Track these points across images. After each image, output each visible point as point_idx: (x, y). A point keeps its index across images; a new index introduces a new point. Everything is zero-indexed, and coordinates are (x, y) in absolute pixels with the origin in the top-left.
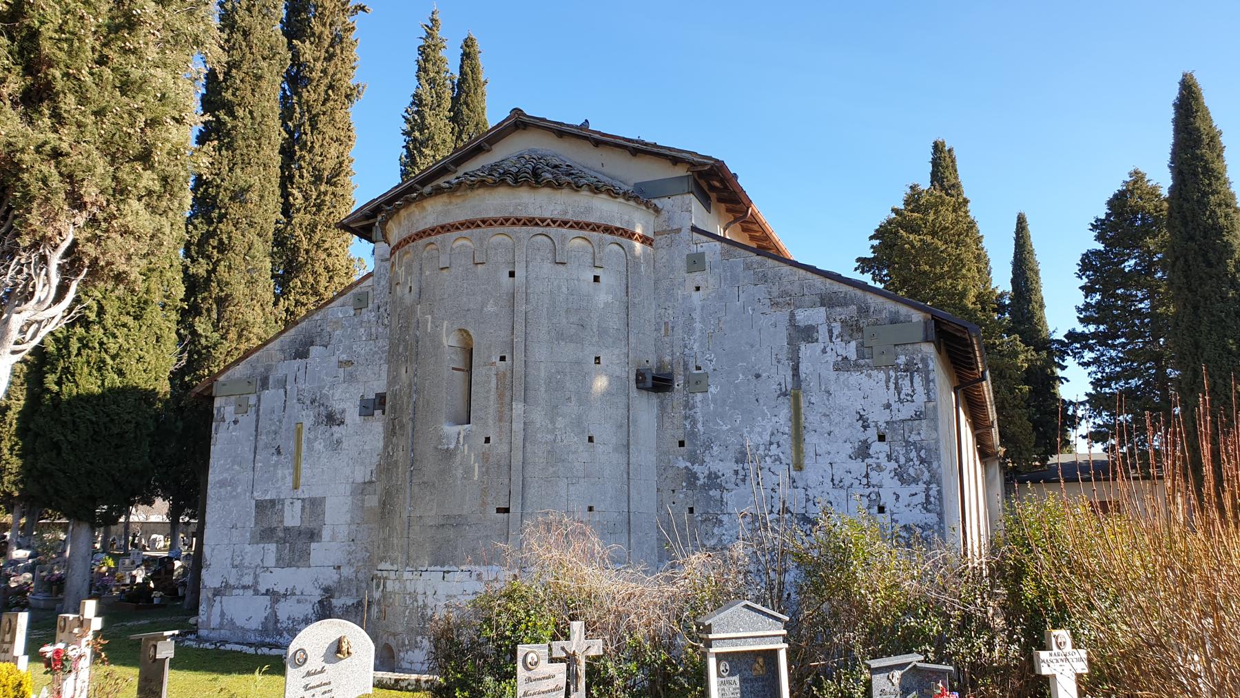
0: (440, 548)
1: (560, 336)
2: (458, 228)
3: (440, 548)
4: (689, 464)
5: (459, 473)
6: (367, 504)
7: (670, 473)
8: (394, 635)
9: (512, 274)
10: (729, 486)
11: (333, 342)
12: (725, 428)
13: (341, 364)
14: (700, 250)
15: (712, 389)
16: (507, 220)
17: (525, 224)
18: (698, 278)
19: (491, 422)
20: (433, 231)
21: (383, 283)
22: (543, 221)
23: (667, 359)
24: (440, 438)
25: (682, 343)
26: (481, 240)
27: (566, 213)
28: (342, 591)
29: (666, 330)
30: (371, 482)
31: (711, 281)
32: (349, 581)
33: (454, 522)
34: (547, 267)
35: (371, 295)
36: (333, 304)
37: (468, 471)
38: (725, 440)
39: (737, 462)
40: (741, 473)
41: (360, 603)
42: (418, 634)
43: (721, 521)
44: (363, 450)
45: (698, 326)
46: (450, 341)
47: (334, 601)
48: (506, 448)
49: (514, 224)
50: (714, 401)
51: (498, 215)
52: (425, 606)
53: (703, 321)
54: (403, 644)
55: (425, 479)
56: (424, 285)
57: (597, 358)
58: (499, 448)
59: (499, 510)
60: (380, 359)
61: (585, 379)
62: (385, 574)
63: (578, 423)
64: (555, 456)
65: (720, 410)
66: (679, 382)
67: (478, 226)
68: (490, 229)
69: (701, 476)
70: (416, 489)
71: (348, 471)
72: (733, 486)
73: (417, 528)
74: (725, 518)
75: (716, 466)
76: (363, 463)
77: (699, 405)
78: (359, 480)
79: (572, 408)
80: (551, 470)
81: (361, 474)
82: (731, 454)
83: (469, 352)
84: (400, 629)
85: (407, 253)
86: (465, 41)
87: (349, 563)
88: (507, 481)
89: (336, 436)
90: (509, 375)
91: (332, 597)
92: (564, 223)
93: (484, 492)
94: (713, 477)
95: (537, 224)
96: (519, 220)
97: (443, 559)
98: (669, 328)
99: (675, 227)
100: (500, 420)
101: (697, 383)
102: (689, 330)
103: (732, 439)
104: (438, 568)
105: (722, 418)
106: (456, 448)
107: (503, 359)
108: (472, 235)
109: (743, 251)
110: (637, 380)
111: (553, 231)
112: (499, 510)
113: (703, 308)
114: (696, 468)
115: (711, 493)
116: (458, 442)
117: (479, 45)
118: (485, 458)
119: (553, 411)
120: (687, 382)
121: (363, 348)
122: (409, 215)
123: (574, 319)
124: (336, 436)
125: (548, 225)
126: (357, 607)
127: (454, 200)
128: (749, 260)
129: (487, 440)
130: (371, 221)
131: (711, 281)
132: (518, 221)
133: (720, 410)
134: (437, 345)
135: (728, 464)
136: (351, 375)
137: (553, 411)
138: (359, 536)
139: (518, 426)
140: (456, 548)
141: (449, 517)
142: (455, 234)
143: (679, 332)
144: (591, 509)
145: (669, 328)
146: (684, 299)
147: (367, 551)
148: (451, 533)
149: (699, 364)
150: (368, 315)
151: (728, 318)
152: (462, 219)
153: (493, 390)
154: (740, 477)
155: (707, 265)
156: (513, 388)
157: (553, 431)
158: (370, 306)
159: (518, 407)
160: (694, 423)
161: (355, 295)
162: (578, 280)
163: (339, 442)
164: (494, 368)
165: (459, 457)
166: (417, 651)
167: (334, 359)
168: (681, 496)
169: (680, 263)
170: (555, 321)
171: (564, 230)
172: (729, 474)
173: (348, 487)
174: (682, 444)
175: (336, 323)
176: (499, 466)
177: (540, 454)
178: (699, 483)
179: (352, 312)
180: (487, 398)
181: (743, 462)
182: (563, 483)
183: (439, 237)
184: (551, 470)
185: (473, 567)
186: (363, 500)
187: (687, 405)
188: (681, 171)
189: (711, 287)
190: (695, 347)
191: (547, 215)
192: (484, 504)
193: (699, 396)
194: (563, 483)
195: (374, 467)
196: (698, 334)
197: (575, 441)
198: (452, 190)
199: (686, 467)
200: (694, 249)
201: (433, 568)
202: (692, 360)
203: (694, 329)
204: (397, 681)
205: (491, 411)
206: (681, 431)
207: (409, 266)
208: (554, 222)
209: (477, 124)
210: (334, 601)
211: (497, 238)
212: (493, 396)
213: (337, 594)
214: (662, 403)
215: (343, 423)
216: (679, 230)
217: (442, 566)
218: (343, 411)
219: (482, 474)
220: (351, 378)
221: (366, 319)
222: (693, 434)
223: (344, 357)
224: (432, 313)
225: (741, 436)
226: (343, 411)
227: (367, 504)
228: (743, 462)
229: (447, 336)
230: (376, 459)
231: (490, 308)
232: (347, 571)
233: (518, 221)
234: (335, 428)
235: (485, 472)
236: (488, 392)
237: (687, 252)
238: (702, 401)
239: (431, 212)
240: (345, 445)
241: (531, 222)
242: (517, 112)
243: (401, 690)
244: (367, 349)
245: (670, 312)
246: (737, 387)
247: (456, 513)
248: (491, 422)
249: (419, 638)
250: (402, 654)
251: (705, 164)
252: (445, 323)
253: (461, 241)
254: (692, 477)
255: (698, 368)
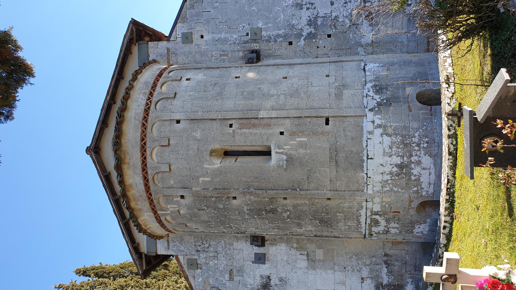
0: (351, 164)
1: (220, 94)
2: (145, 158)
3: (351, 164)
4: (303, 38)
5: (302, 151)
6: (322, 258)
7: (307, 50)
8: (411, 202)
9: (178, 122)
10: (315, 12)
11: (217, 285)
12: (282, 17)
13: (231, 279)
14: (180, 36)
15: (260, 25)
16: (144, 125)
17: (148, 115)
18: (196, 37)
19: (270, 131)
20: (146, 179)
21: (182, 248)
22: (147, 104)
23: (241, 54)
24: (279, 167)
25: (233, 45)
26: (154, 141)
27: (145, 93)
28: (378, 276)
29: (224, 55)
30: (308, 255)
31: (198, 28)
32: (371, 271)
33: (334, 152)
34: (176, 102)
35: (189, 257)
36: (193, 285)
37: (302, 145)
38: (289, 16)
39: (302, 9)
40: (308, 6)
41: (386, 262)
42: (410, 179)
43: (336, 17)
44: (287, 261)
45: (223, 36)
46: (217, 163)
47: (385, 282)
48: (287, 121)
49: (146, 121)
50: (266, 24)
51: (140, 130)
52: (391, 173)
53: (220, 33)
54: (417, 192)
55: (305, 178)
56: (180, 185)
57: (236, 78)
58: (287, 125)
59: (327, 123)
60: (230, 249)
61: (248, 82)
62: (369, 214)
63: (275, 84)
64: (294, 93)
65: (272, 20)
66: (255, 46)
67: (145, 144)
68: (148, 135)
69: (309, 31)
70: (312, 185)
71: (300, 272)
72: (316, 10)
73: (338, 183)
74: (334, 14)
75: (304, 21)
76: (295, 261)
77: (268, 33)
78: (305, 264)
79: (265, 88)
80: (302, 95)
81: (303, 263)
82: (298, 12)
83: (227, 154)
84: (407, 195)
85: (159, 202)
86: (77, 274)
87: (359, 271)
88: (308, 119)
89: (277, 282)
90: (241, 121)
91: (382, 284)
92: (151, 94)
93: (315, 133)
94: (310, 23)
95: (149, 108)
96: (145, 117)
97: (358, 162)
98: (224, 53)
99: (166, 52)
100: (269, 125)
101: (256, 35)
102: (224, 41)
103: (289, 12)
104: (365, 164)
105: (277, 19)
106: (286, 154)
107: (231, 126)
108: (150, 147)
109: (183, 10)
110: (251, 63)
111: (154, 99)
112: (327, 123)
113: (213, 33)
114: (305, 34)
115: (319, 24)
116: (282, 153)
117: (81, 267)
118: (293, 134)
119: (267, 96)
120: (255, 41)
121: (222, 263)
122: (135, 200)
123: (211, 88)
124: (277, 282)
125: (151, 102)
126: (388, 264)
127: (127, 161)
128: (189, 6)
129: (282, 133)
130: (143, 256)
131: (198, 28)
132: (145, 119)
133: (272, 20)
134: (219, 172)
135: (303, 14)
136: (239, 271)
137: (267, 96)
138: (342, 264)
139: (274, 114)
140: (352, 152)
141: (331, 158)
142: (148, 158)
143: (226, 47)
144: (327, 76)
145: (224, 53)
146: (207, 45)
147: (351, 257)
148: (342, 155)
149: (245, 34)
150: (201, 259)
151: (220, 17)
152: (139, 155)
153: (251, 131)
154: (310, 6)
155: (189, 31)
156: (249, 120)
157: (279, 96)
158: (196, 257)
159: (262, 114)
160: (278, 36)
161: (188, 269)
162: (187, 87)
163: (281, 280)
164: (236, 131)
165: (293, 152)
166: (422, 179)
167: (228, 284)
168: (321, 42)
169: (187, 48)
170: (210, 97)
171: (155, 93)
172: (308, 13)
173: (310, 272)
174: (291, 43)
175: (205, 283)
176: (299, 125)
177: (292, 101)
178: (313, 31)
179: (199, 271)
180: (255, 134)
181: (302, 5)
182: (311, 89)
183: (149, 172)
184: (302, 95)
185: (365, 139)
186: (319, 260)
187: (268, 41)
188: (135, 49)
189: (202, 28)
190: (235, 36)
191: (144, 102)
192: (323, 133)
193: (264, 33)
194: (311, 89)
195: (298, 253)
196: (228, 35)
197: (284, 86)
198: (119, 167)
199: (304, 40)
200: (179, 40)
201: (365, 169)
202: (242, 38)
203: (224, 38)
204: (450, 154)
205: (263, 131)
206: (283, 44)
207: (168, 202)
208: (149, 98)
209: (122, 268)
210: (385, 282)
211: (154, 132)
212: (254, 131)
213: (380, 280)
214: (266, 57)
215: (269, 277)
216: (168, 49)
217: (363, 161)
218: (261, 276)
219: (304, 135)
220: (241, 271)
221: (204, 260)
222: (285, 36)
223: (227, 276)
224: (198, 177)
225: (287, 6)
226: (261, 276)
227: (322, 258)
228: (302, 5)
229: (214, 164)
230: (293, 252)
231: (198, 135)
232: (365, 273)
233: (145, 119)
234: (272, 283)
235: (302, 133)
236: (251, 134)
237: (181, 43)
238: (266, 31)
239: (134, 178)
240: (283, 275)
241: (147, 111)
242: (88, 150)
243: (456, 150)
244: (223, 259)
245: (214, 53)
246: (259, 10)
247: (328, 153)
248: (270, 131)
249: (413, 178)
250: (424, 193)
251: (132, 30)
252: (205, 166)
253: (154, 157)
254: (310, 36)
255: (247, 34)
